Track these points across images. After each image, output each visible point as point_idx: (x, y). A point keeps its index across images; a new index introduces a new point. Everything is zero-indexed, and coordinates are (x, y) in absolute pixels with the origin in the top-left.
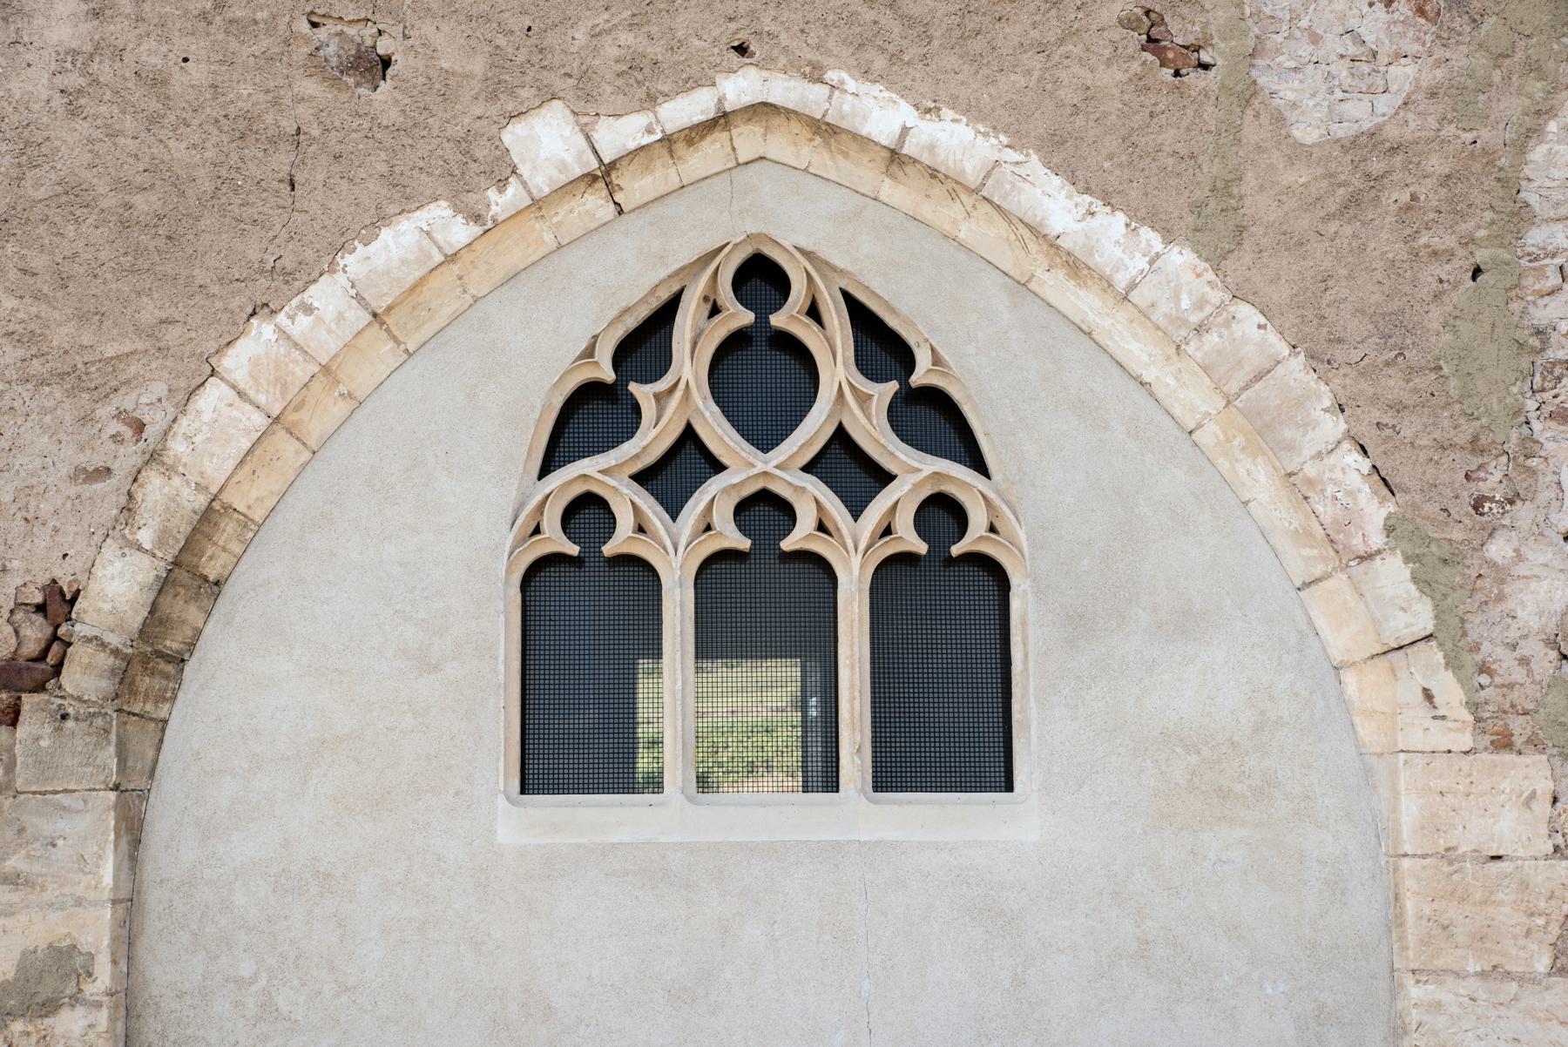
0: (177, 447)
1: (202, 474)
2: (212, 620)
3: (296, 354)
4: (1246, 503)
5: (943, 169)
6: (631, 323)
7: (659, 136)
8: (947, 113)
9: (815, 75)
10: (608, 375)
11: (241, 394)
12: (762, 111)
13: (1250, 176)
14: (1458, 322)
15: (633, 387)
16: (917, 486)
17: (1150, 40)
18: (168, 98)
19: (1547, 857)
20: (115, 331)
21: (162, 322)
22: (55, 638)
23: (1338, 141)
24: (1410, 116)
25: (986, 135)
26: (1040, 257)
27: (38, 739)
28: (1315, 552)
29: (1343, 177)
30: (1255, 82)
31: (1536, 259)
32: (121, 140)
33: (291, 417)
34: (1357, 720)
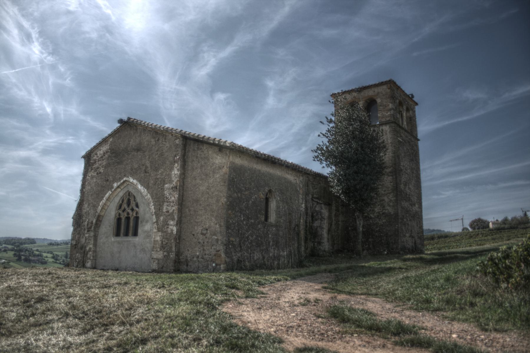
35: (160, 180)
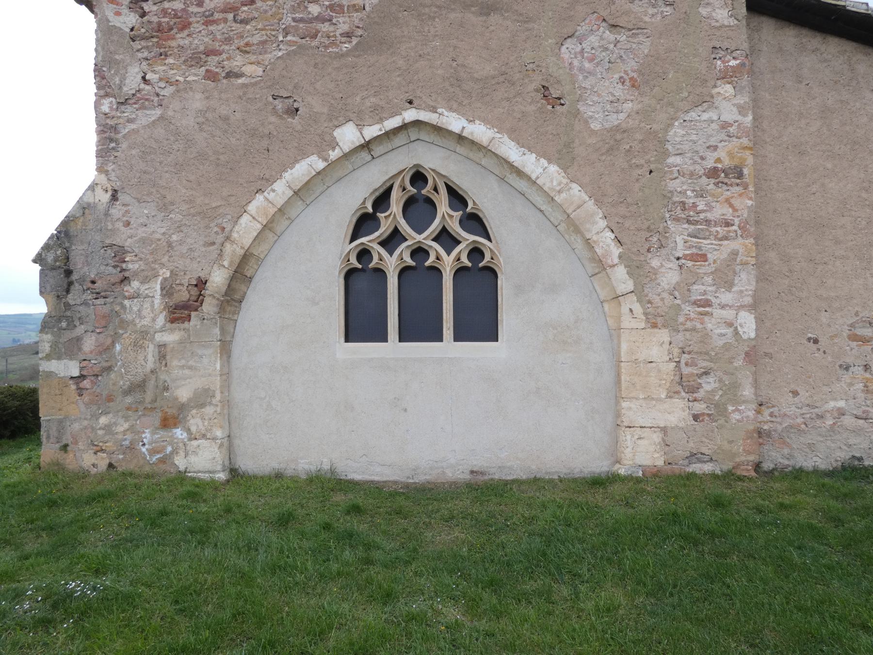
0: (235, 235)
1: (242, 243)
2: (249, 289)
3: (270, 205)
4: (574, 249)
5: (475, 141)
6: (377, 194)
7: (383, 132)
8: (477, 122)
9: (434, 110)
10: (370, 210)
11: (254, 218)
12: (417, 123)
13: (577, 141)
14: (644, 189)
15: (378, 214)
16: (467, 245)
17: (544, 96)
18: (230, 124)
19: (667, 362)
20: (215, 199)
21: (229, 196)
22: (200, 295)
23: (606, 129)
24: (630, 120)
25: (490, 129)
26: (508, 169)
27: (196, 326)
28: (596, 265)
29: (607, 141)
30: (579, 110)
31: (670, 168)
32: (216, 138)
33: (270, 225)
34: (608, 319)
35: (638, 136)
